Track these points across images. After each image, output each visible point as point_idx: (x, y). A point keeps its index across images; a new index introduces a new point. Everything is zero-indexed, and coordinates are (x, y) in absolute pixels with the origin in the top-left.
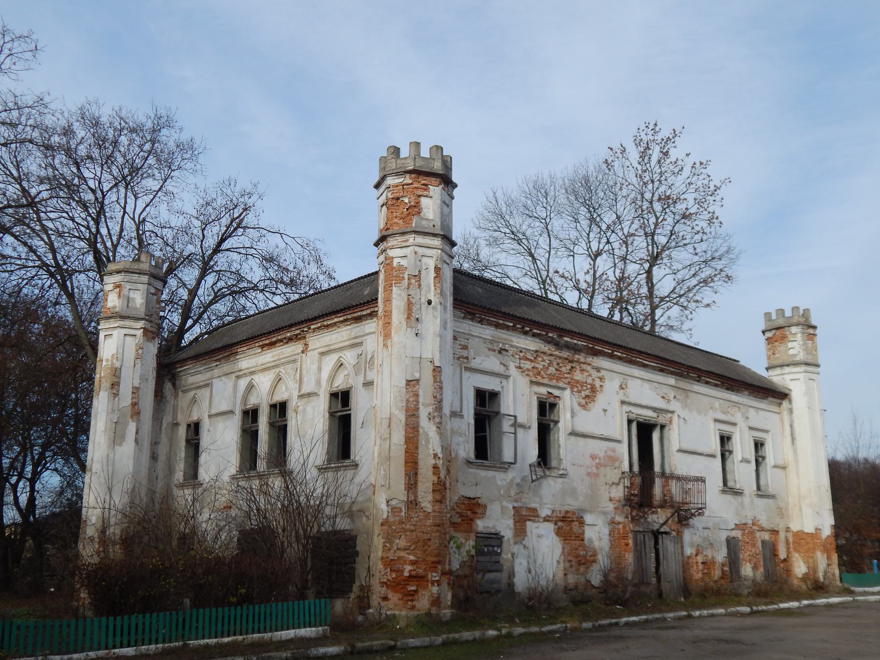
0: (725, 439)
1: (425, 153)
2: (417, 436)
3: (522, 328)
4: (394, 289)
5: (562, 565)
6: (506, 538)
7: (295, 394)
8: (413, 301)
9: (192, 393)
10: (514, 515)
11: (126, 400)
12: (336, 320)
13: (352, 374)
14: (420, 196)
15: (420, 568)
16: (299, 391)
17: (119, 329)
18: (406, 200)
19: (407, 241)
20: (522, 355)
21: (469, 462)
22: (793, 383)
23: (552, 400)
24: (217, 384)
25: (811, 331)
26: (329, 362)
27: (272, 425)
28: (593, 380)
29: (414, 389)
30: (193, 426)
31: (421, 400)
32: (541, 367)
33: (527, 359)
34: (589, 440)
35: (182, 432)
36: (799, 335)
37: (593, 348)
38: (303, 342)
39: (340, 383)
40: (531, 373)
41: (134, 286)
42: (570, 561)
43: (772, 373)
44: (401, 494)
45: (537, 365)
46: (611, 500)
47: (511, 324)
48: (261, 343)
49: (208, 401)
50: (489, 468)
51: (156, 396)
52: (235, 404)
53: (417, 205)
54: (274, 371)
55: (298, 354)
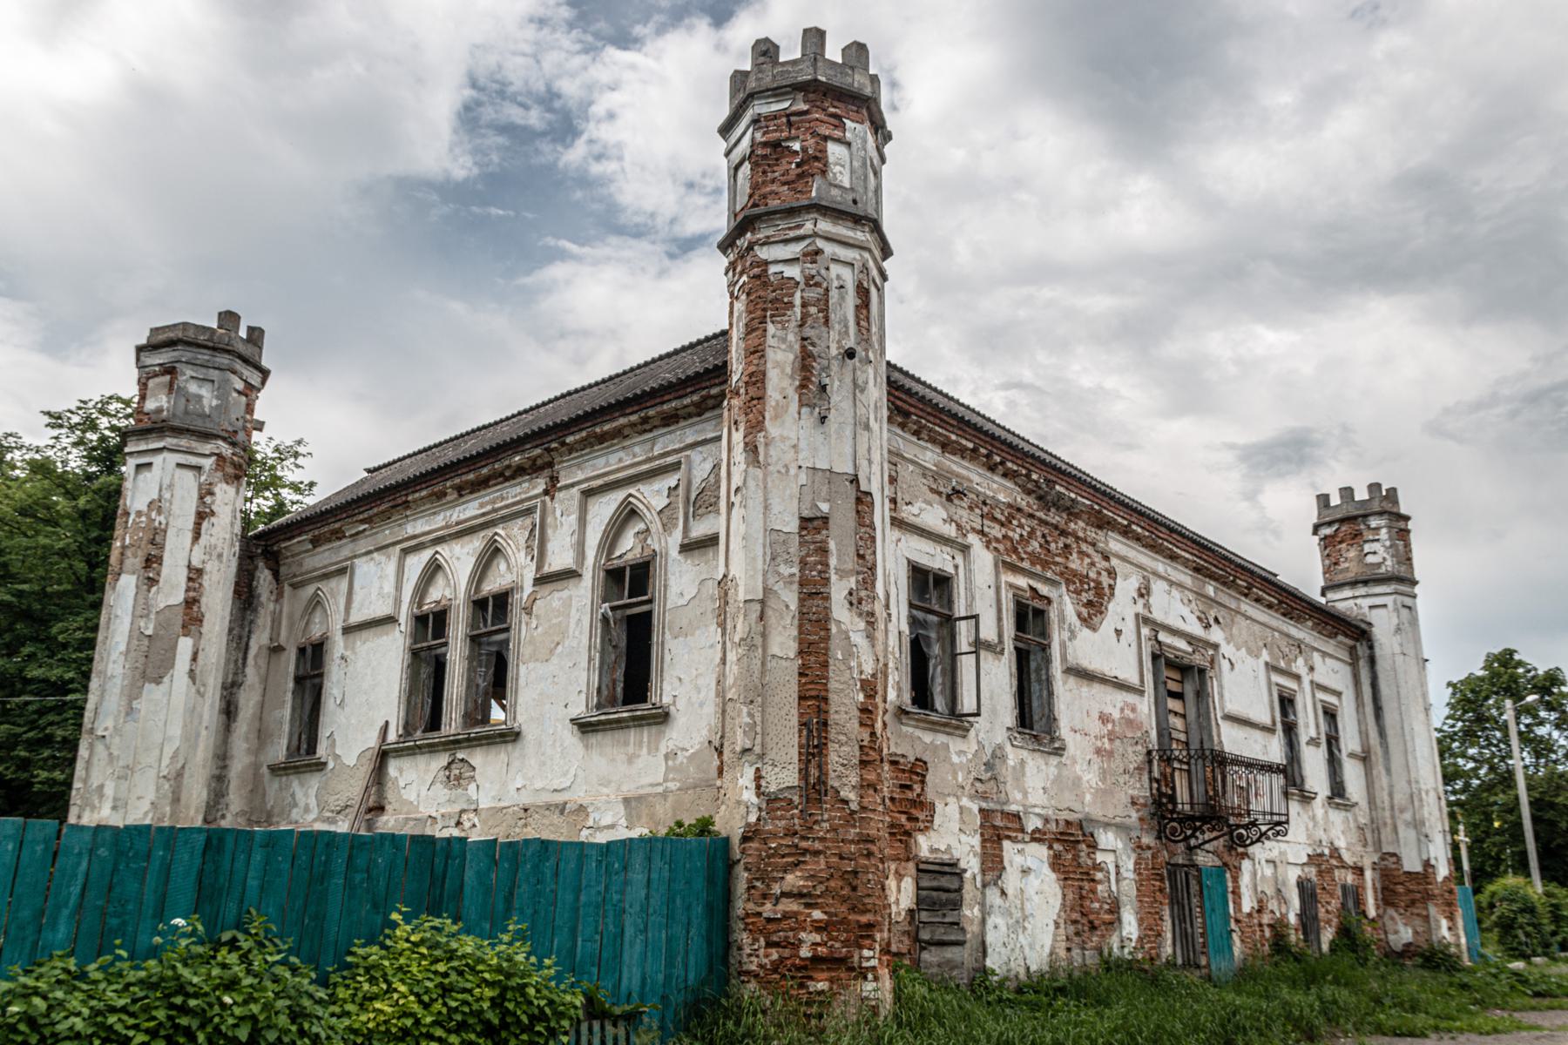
0: (1286, 702)
1: (833, 53)
2: (827, 638)
3: (988, 456)
4: (771, 329)
5: (1062, 931)
6: (968, 875)
7: (530, 574)
8: (815, 351)
9: (310, 589)
10: (982, 826)
11: (172, 591)
12: (622, 421)
13: (656, 526)
14: (826, 138)
15: (836, 939)
16: (539, 568)
17: (166, 454)
18: (796, 146)
19: (799, 227)
20: (986, 509)
21: (901, 712)
22: (1374, 611)
23: (1037, 604)
24: (364, 568)
25: (1402, 525)
26: (604, 509)
27: (475, 640)
28: (1099, 573)
29: (819, 537)
30: (309, 650)
31: (833, 562)
32: (1017, 537)
33: (994, 519)
34: (1097, 688)
35: (289, 661)
36: (1384, 531)
37: (1100, 512)
38: (547, 472)
39: (628, 546)
40: (1001, 547)
41: (201, 373)
42: (1075, 922)
43: (1331, 596)
44: (784, 776)
45: (1011, 534)
46: (1134, 803)
47: (971, 445)
48: (457, 481)
49: (342, 601)
50: (934, 727)
51: (237, 593)
52: (398, 602)
53: (820, 157)
54: (482, 534)
55: (536, 497)
